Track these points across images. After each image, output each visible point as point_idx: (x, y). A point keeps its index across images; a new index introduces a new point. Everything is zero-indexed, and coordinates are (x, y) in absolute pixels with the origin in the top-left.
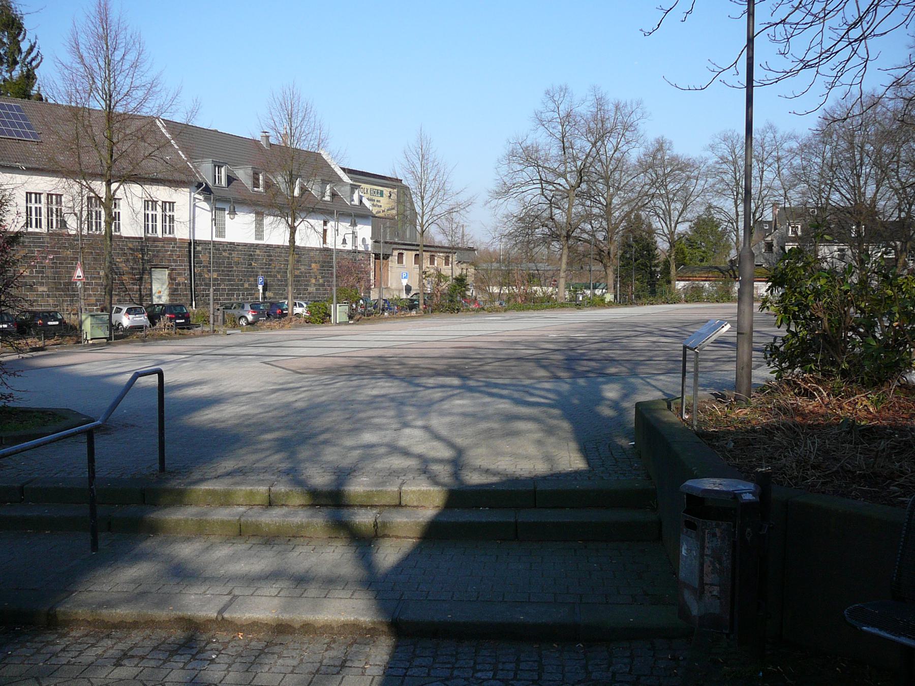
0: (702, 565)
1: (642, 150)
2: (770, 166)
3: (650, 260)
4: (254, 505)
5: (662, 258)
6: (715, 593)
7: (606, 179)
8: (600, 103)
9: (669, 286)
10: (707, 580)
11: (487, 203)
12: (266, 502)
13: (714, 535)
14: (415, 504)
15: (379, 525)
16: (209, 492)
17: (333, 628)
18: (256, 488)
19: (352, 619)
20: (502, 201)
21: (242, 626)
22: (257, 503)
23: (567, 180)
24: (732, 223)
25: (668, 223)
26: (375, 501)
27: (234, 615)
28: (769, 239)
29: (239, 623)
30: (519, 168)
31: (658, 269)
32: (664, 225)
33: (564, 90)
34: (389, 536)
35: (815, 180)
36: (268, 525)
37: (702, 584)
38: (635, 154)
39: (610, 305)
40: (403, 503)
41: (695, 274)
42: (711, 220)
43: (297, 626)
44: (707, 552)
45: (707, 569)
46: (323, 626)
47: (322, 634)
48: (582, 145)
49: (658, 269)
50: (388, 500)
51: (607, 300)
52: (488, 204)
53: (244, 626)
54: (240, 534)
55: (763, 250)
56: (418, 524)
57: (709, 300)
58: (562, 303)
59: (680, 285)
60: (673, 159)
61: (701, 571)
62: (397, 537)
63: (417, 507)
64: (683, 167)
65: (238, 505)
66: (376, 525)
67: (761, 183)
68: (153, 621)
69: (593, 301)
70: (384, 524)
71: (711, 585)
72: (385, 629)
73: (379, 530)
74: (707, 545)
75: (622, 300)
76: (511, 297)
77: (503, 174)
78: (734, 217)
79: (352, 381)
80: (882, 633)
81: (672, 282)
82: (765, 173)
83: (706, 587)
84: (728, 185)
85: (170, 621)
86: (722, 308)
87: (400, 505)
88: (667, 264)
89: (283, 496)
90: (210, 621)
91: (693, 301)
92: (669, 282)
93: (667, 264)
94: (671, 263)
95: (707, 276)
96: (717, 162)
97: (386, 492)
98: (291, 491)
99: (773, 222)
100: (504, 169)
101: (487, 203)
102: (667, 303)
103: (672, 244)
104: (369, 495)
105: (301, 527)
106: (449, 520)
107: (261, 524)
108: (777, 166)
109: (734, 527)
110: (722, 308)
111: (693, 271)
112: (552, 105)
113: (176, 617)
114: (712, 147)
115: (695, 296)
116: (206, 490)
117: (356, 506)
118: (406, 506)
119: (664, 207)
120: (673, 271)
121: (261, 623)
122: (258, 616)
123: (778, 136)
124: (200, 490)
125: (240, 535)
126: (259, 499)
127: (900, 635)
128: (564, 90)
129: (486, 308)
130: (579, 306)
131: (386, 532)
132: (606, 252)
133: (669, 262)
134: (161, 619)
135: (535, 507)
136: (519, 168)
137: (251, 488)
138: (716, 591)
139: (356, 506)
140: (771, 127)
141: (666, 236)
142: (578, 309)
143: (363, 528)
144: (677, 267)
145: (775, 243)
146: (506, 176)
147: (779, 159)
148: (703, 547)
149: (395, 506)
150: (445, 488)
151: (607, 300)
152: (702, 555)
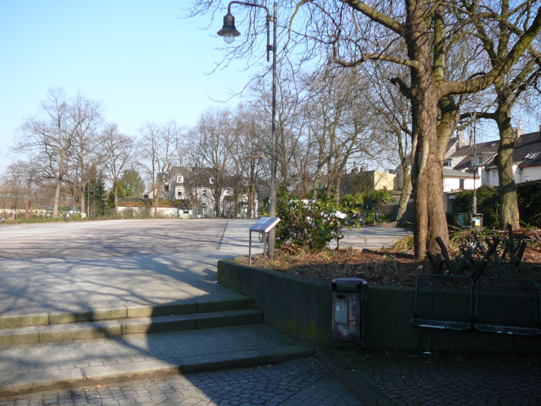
0: (348, 313)
1: (103, 129)
2: (172, 143)
3: (101, 194)
4: (39, 325)
5: (108, 193)
6: (354, 324)
7: (82, 146)
8: (79, 99)
9: (114, 209)
10: (351, 319)
11: (7, 154)
12: (47, 323)
13: (353, 300)
14: (136, 316)
15: (123, 328)
16: (8, 320)
17: (149, 375)
18: (40, 314)
19: (160, 368)
20: (17, 154)
21: (98, 381)
22: (41, 324)
23: (60, 144)
24: (151, 174)
25: (114, 172)
26: (113, 316)
27: (94, 376)
28: (166, 184)
29: (96, 380)
30: (30, 134)
31: (105, 200)
32: (111, 173)
33: (60, 90)
34: (129, 333)
35: (336, 153)
36: (57, 334)
37: (348, 321)
38: (99, 131)
39: (85, 220)
40: (129, 316)
41: (128, 202)
42: (134, 172)
43: (130, 377)
44: (350, 307)
45: (350, 314)
46: (144, 375)
47: (144, 379)
48: (70, 124)
49: (105, 200)
50: (121, 315)
51: (83, 217)
52: (8, 156)
53: (99, 381)
54: (39, 341)
55: (163, 190)
56: (144, 325)
57: (137, 217)
58: (56, 219)
59: (120, 209)
60: (120, 137)
61: (348, 316)
62: (134, 333)
63: (137, 317)
64: (125, 141)
65: (28, 326)
66: (122, 328)
67: (167, 151)
68: (42, 387)
69: (75, 217)
70: (126, 327)
71: (352, 321)
72: (177, 371)
73: (124, 330)
74: (350, 304)
75: (91, 218)
76: (21, 215)
77: (63, 137)
78: (152, 170)
79: (178, 238)
80: (429, 326)
81: (116, 207)
82: (169, 147)
83: (350, 322)
84: (149, 152)
85: (53, 385)
86: (144, 222)
87: (127, 317)
88: (112, 197)
89: (58, 318)
90: (79, 381)
91: (128, 218)
92: (114, 207)
93: (112, 197)
94: (115, 196)
95: (135, 203)
96: (143, 139)
97: (119, 311)
98: (63, 314)
99: (168, 175)
100: (20, 134)
101: (7, 154)
102: (114, 219)
103: (115, 185)
104: (109, 313)
105: (77, 333)
106: (161, 321)
107: (52, 334)
108: (176, 143)
109: (361, 295)
110: (144, 222)
111: (127, 201)
112: (53, 99)
113: (57, 382)
114: (141, 130)
115: (129, 215)
116: (7, 318)
117: (102, 320)
118: (130, 317)
119: (111, 163)
120: (116, 200)
121: (109, 378)
122: (107, 374)
123: (177, 128)
124: (2, 319)
125: (39, 342)
126: (42, 321)
127: (435, 325)
128: (60, 90)
129: (5, 222)
130: (66, 220)
131: (128, 331)
132: (81, 188)
133: (114, 195)
134: (48, 384)
135: (198, 312)
136: (30, 134)
137: (37, 315)
138: (354, 323)
139: (102, 320)
140: (174, 122)
141: (112, 179)
142: (66, 222)
143: (115, 330)
144: (118, 198)
145: (170, 186)
146: (20, 138)
147: (177, 140)
148: (348, 305)
149: (124, 318)
150: (151, 306)
151: (83, 217)
152: (348, 309)
